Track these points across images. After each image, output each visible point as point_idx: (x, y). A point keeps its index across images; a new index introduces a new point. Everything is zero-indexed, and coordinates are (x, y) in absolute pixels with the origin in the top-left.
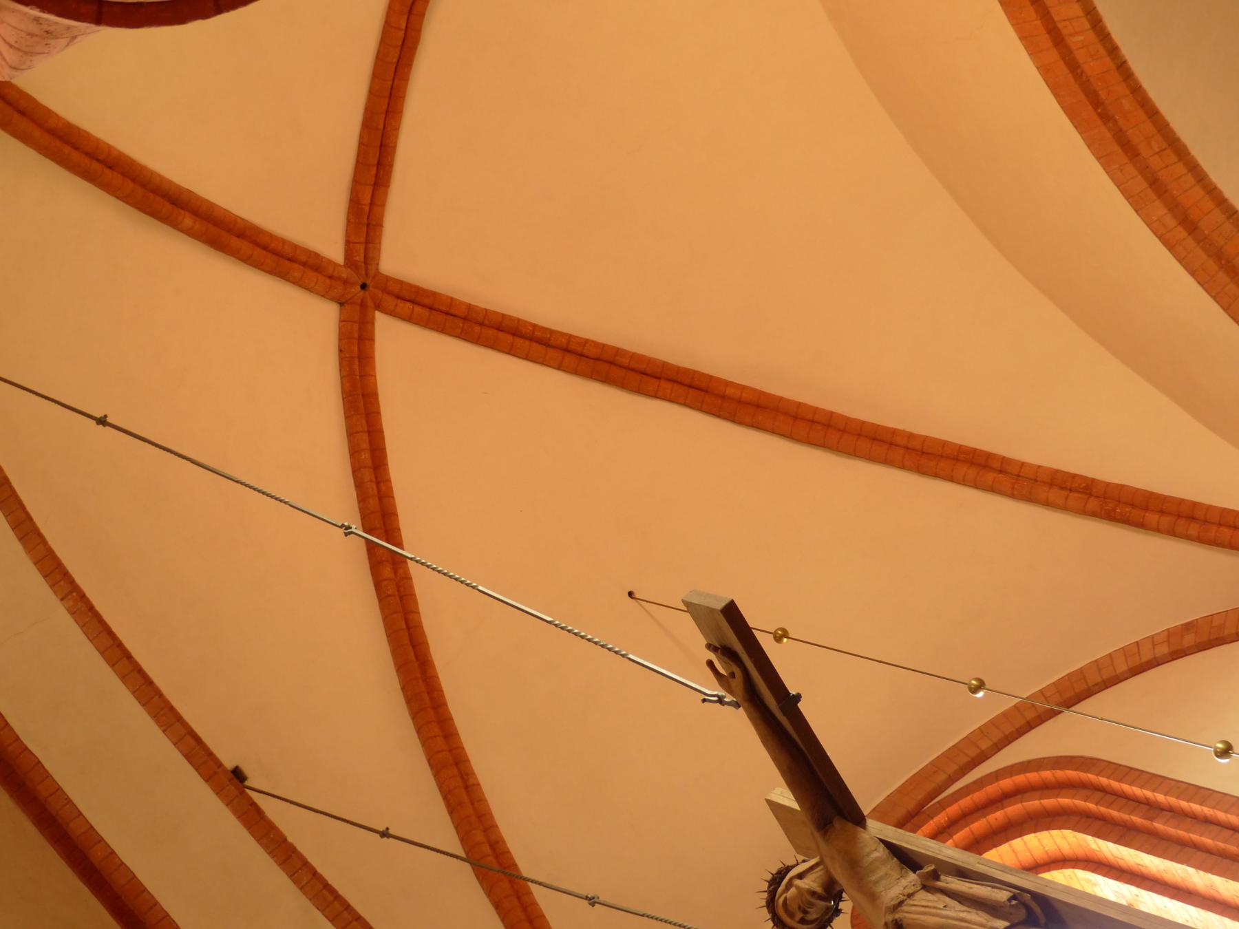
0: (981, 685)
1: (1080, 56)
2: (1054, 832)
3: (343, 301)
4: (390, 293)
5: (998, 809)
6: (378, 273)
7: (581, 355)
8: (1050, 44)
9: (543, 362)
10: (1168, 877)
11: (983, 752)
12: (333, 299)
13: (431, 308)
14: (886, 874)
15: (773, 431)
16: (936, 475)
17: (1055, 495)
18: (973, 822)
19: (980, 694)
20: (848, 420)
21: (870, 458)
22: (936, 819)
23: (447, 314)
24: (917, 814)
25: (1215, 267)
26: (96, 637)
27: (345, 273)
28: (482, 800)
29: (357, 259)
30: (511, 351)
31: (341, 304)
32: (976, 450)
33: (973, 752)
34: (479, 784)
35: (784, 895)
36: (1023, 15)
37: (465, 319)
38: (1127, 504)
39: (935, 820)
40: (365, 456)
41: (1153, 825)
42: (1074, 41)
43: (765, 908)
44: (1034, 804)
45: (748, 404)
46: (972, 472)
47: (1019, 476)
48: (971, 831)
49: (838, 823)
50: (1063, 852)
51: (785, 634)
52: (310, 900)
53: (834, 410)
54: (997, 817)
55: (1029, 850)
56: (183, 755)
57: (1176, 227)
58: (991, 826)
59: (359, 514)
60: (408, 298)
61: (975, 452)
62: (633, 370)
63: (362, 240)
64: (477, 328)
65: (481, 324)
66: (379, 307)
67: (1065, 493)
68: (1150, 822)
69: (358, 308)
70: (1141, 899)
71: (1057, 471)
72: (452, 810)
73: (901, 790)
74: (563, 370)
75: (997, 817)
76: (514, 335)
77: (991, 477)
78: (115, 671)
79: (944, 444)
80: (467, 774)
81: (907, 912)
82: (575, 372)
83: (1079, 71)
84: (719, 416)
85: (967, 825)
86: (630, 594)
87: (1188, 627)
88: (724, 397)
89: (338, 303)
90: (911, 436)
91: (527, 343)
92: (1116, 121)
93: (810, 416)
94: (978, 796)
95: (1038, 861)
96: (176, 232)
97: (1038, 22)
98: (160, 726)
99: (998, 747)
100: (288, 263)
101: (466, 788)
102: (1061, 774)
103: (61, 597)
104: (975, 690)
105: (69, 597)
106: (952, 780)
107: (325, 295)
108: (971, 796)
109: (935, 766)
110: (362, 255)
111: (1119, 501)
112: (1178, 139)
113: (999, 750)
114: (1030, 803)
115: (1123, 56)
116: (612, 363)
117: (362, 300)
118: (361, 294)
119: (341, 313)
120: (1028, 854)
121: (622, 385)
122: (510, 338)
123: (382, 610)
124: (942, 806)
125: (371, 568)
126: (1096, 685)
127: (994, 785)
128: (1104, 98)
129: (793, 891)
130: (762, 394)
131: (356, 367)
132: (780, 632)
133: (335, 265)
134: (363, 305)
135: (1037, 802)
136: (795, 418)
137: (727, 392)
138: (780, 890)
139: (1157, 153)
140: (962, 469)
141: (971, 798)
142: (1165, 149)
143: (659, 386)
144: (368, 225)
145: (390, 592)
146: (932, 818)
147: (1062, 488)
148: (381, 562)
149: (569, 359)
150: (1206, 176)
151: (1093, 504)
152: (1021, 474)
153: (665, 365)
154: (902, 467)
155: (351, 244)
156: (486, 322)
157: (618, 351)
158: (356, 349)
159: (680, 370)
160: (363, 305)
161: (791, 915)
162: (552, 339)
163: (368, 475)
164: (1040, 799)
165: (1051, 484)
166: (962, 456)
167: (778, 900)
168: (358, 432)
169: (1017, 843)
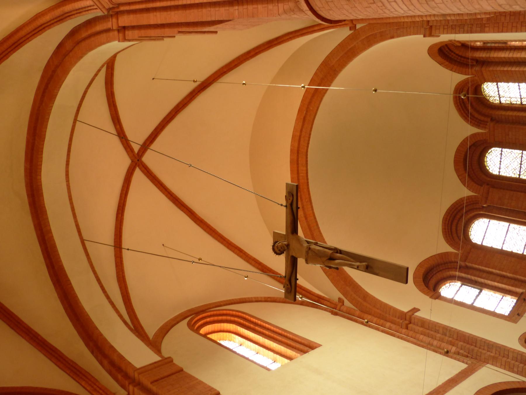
1: (300, 178)
9: (164, 193)
17: (253, 263)
27: (136, 156)
30: (159, 188)
31: (132, 161)
33: (219, 304)
40: (125, 192)
44: (229, 318)
46: (238, 252)
49: (295, 234)
51: (201, 259)
54: (220, 318)
55: (224, 327)
66: (139, 166)
75: (220, 318)
77: (242, 254)
79: (235, 245)
82: (169, 198)
86: (163, 245)
87: (269, 298)
94: (218, 312)
96: (114, 127)
102: (237, 313)
104: (246, 277)
106: (213, 308)
107: (130, 158)
109: (210, 304)
112: (311, 201)
118: (137, 161)
119: (131, 163)
122: (160, 185)
124: (210, 311)
129: (280, 244)
131: (130, 175)
133: (135, 153)
134: (136, 164)
136: (208, 227)
138: (276, 244)
149: (169, 195)
151: (260, 267)
154: (225, 246)
157: (179, 198)
160: (136, 164)
165: (253, 260)
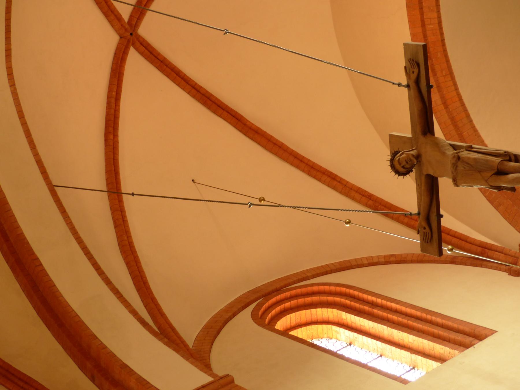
0: (349, 222)
2: (329, 310)
3: (122, 36)
4: (139, 41)
5: (310, 297)
6: (137, 32)
7: (198, 91)
8: (420, 25)
9: (183, 89)
10: (372, 331)
11: (308, 276)
12: (119, 34)
13: (151, 53)
14: (449, 149)
15: (259, 143)
16: (314, 177)
18: (299, 299)
19: (348, 225)
20: (288, 148)
21: (292, 164)
22: (286, 293)
23: (156, 57)
24: (279, 290)
25: (450, 123)
26: (17, 105)
27: (127, 26)
28: (128, 227)
29: (133, 23)
31: (121, 38)
32: (332, 172)
34: (127, 221)
35: (399, 157)
36: (414, 12)
37: (161, 62)
38: (383, 206)
39: (286, 294)
40: (114, 94)
41: (373, 310)
42: (429, 27)
43: (389, 161)
45: (253, 130)
46: (329, 179)
47: (345, 186)
48: (298, 302)
49: (428, 135)
50: (329, 319)
52: (69, 229)
53: (284, 143)
56: (36, 161)
57: (441, 105)
58: (305, 302)
59: (105, 114)
60: (144, 45)
61: (331, 173)
62: (215, 103)
63: (137, 17)
64: (165, 67)
65: (167, 66)
66: (133, 45)
67: (361, 196)
68: (372, 309)
69: (127, 41)
70: (357, 339)
71: (360, 188)
72: (116, 226)
73: (274, 281)
74: (190, 95)
75: (309, 299)
76: (177, 74)
77: (335, 183)
78: (20, 121)
79: (321, 167)
80: (125, 216)
81: (462, 154)
82: (194, 97)
83: (426, 38)
84: (240, 131)
85: (297, 299)
86: (193, 180)
87: (392, 256)
88: (245, 125)
89: (120, 36)
90: (309, 160)
91: (180, 79)
92: (432, 61)
93: (274, 142)
94: (304, 290)
95: (318, 320)
97: (419, 16)
98: (30, 147)
99: (314, 277)
100: (111, 12)
101: (123, 221)
102: (338, 289)
103: (11, 85)
105: (13, 86)
106: (294, 283)
108: (301, 289)
109: (288, 277)
110: (135, 22)
111: (380, 204)
112: (453, 73)
113: (314, 278)
114: (323, 297)
115: (444, 37)
116: (209, 98)
117: (129, 39)
118: (129, 36)
119: (120, 40)
120: (316, 316)
121: (209, 108)
123: (105, 149)
124: (290, 290)
125: (105, 134)
126: (355, 265)
127: (311, 287)
128: (431, 51)
129: (404, 155)
130: (259, 128)
131: (119, 62)
132: (262, 198)
134: (129, 41)
135: (325, 297)
137: (247, 123)
139: (444, 76)
140: (324, 178)
141: (301, 290)
142: (447, 75)
143: (223, 112)
144: (141, 13)
145: (111, 144)
146: (285, 293)
147: (360, 194)
148: (110, 133)
150: (458, 89)
152: (347, 185)
153: (227, 106)
154: (303, 171)
155: (133, 17)
156: (169, 66)
158: (121, 55)
159: (232, 110)
160: (129, 41)
161: (400, 164)
162: (190, 81)
163: (113, 101)
164: (327, 297)
165: (357, 192)
166: (327, 173)
167: (396, 158)
168: (114, 84)
169: (314, 310)
